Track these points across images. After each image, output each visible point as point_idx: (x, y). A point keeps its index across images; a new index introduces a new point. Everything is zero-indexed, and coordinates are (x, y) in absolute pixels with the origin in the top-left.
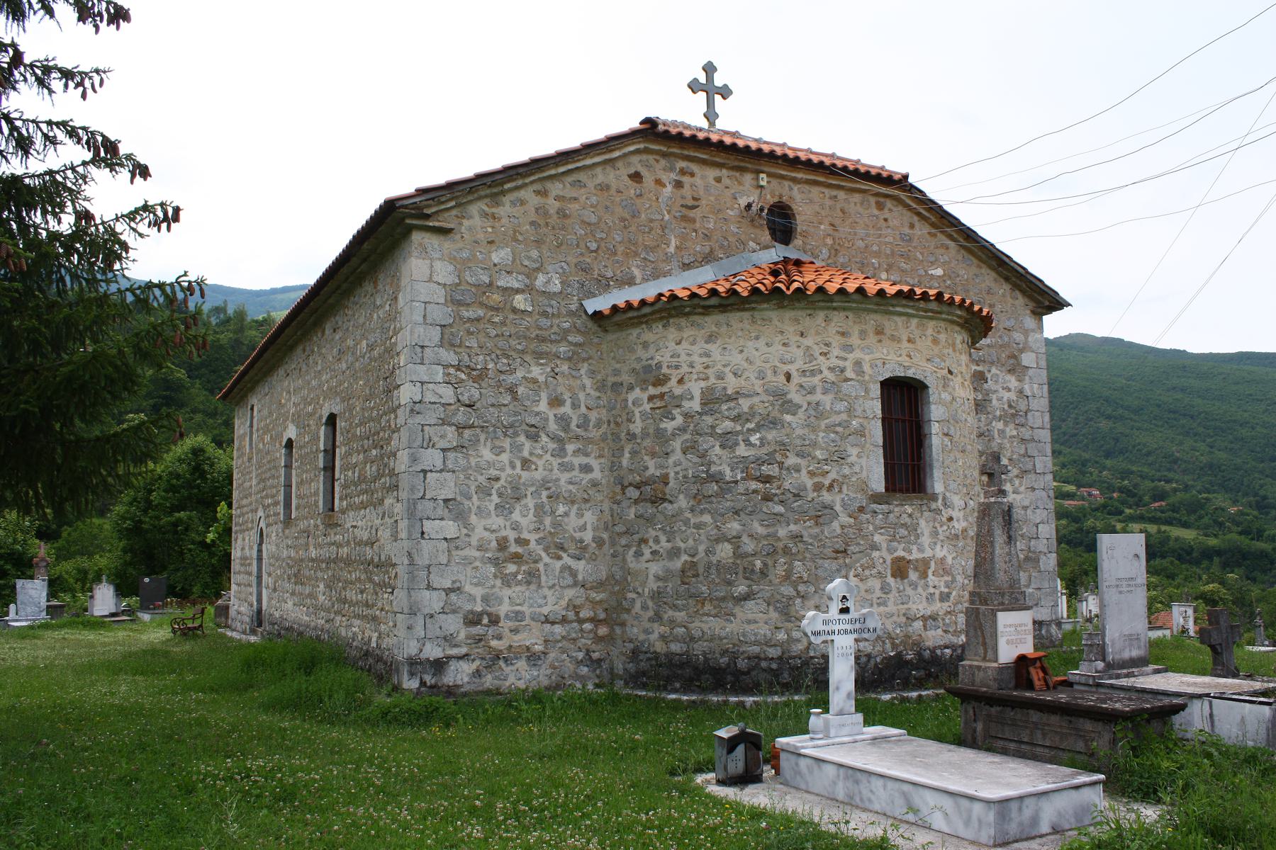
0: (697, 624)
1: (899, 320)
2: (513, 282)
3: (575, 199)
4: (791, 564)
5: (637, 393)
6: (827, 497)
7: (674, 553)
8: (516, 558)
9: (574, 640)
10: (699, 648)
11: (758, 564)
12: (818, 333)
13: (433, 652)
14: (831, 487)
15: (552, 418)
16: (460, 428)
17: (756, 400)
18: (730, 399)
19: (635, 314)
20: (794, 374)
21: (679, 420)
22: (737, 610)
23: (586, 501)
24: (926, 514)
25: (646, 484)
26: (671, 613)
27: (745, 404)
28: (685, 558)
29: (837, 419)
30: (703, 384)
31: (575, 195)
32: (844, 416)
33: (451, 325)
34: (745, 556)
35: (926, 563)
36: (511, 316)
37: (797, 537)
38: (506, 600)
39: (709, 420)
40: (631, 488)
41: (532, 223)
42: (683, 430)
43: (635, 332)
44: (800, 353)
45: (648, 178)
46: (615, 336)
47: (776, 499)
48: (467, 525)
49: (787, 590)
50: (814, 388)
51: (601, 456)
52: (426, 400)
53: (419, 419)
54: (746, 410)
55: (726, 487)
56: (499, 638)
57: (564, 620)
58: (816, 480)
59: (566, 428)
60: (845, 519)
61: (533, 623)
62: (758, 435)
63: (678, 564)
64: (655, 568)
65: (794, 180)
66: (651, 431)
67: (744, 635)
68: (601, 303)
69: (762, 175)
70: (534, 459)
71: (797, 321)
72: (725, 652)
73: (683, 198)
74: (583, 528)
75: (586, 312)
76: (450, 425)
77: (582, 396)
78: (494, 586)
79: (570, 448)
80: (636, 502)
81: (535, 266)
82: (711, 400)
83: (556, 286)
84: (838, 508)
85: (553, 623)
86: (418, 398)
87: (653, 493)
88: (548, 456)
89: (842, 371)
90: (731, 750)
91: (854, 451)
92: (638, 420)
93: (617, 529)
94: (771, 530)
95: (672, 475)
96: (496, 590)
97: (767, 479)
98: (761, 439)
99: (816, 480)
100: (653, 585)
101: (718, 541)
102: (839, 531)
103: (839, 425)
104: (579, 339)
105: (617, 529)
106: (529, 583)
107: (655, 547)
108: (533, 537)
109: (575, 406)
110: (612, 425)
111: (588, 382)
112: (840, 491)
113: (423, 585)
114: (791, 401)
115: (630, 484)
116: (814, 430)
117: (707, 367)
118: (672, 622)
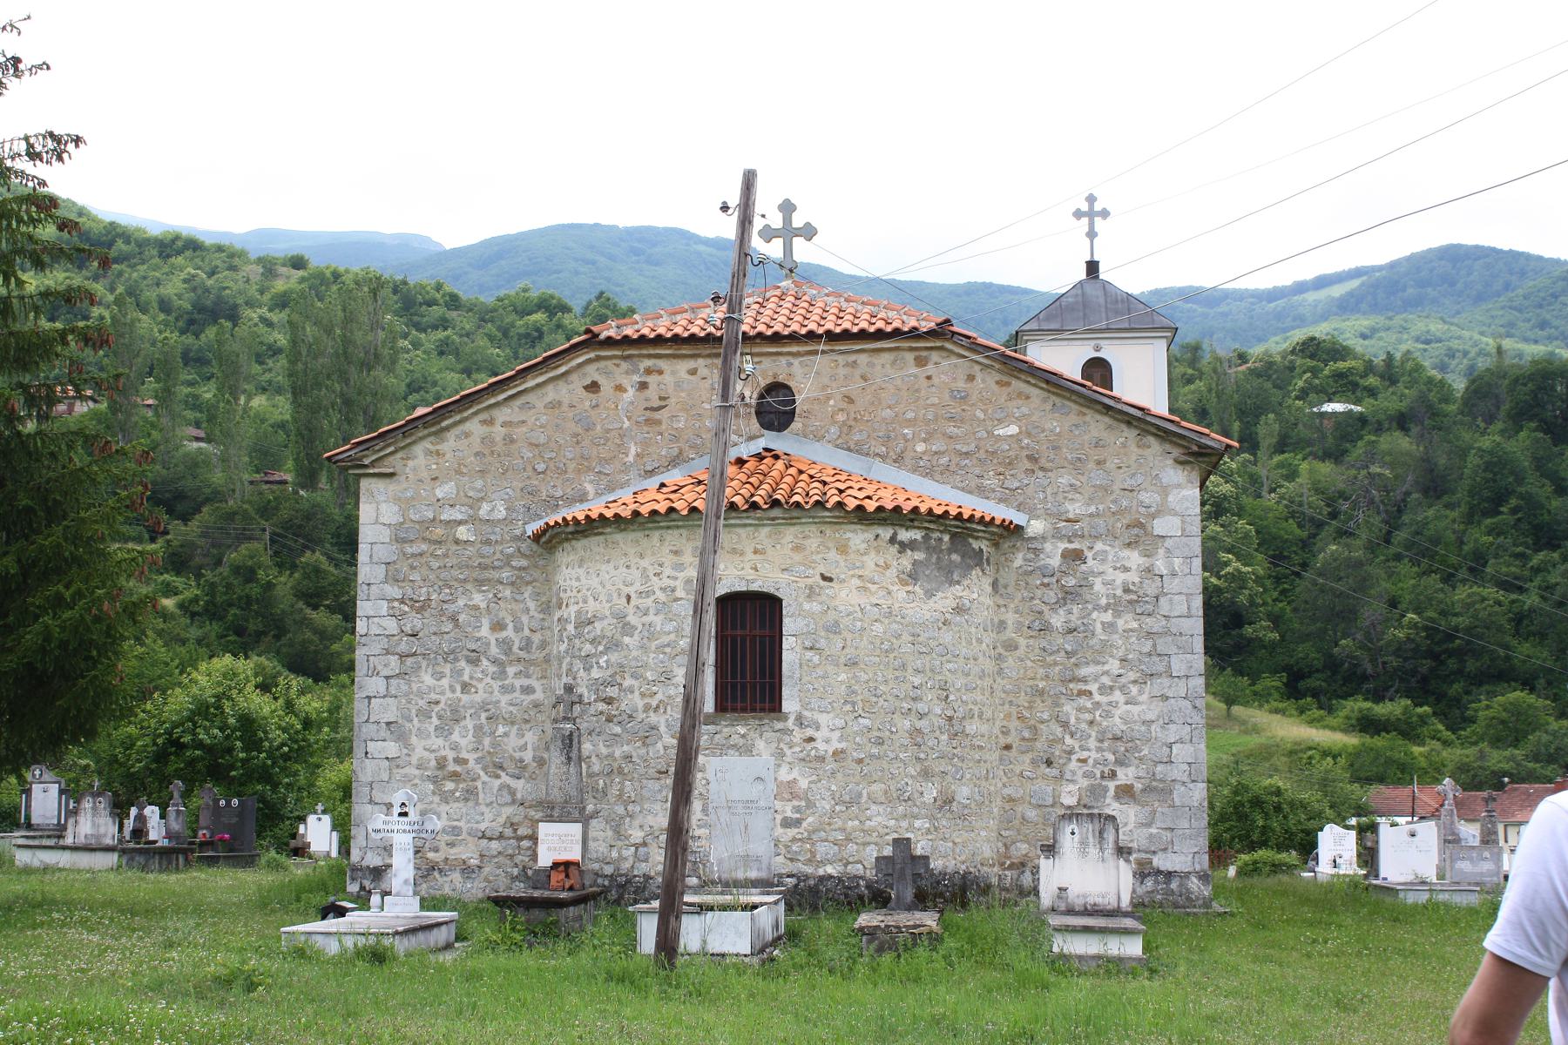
12: (653, 554)
14: (657, 709)
16: (403, 656)
20: (633, 596)
23: (527, 721)
29: (665, 639)
32: (672, 636)
36: (455, 547)
48: (407, 745)
70: (474, 683)
74: (524, 748)
97: (609, 701)
106: (466, 800)
109: (518, 629)
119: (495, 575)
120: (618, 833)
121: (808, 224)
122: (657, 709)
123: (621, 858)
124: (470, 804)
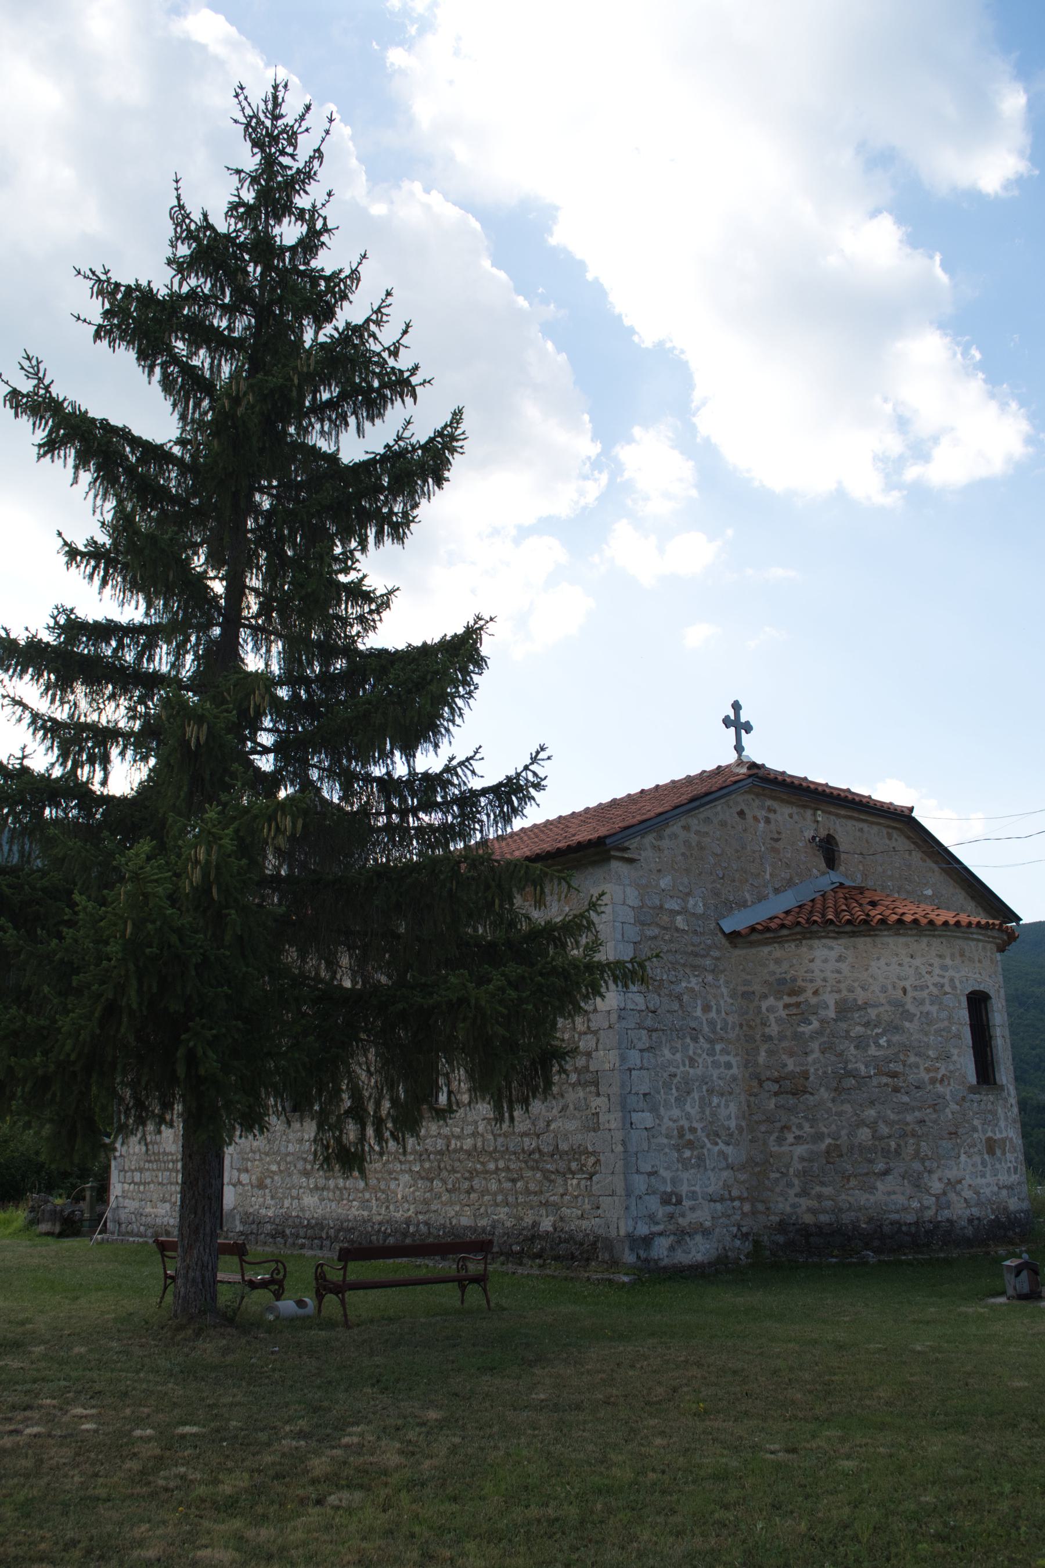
0: (844, 1197)
1: (973, 944)
2: (673, 905)
3: (707, 833)
4: (918, 1145)
5: (771, 1001)
6: (940, 1088)
7: (819, 1137)
8: (690, 1145)
9: (729, 1216)
10: (847, 1218)
11: (893, 1144)
12: (923, 956)
13: (643, 1230)
14: (942, 1081)
15: (705, 1022)
16: (651, 1030)
17: (881, 1009)
18: (860, 1008)
19: (772, 935)
20: (909, 989)
21: (816, 1025)
22: (879, 1184)
23: (730, 1094)
24: (1001, 1102)
25: (785, 1078)
26: (818, 1189)
27: (873, 1013)
28: (828, 1141)
29: (941, 1025)
30: (837, 996)
31: (706, 830)
32: (946, 1023)
33: (639, 943)
34: (881, 1138)
35: (1004, 1140)
36: (676, 935)
37: (921, 1122)
38: (685, 1181)
39: (844, 1026)
40: (769, 1083)
41: (683, 854)
42: (819, 1033)
43: (766, 950)
44: (912, 971)
45: (749, 815)
46: (744, 952)
47: (903, 1090)
48: (659, 1117)
49: (917, 1166)
50: (924, 1000)
51: (737, 1055)
52: (628, 1007)
53: (624, 1024)
54: (874, 1017)
55: (862, 1081)
56: (683, 1215)
57: (722, 1200)
58: (932, 1075)
59: (714, 1032)
60: (954, 1107)
61: (703, 1202)
62: (885, 1038)
63: (823, 1146)
64: (800, 1150)
65: (838, 815)
66: (788, 1034)
67: (886, 1205)
68: (737, 922)
69: (819, 812)
70: (696, 1058)
71: (907, 945)
72: (870, 1220)
73: (771, 832)
74: (729, 1118)
75: (723, 932)
76: (644, 1028)
77: (722, 1002)
78: (678, 1170)
79: (718, 1047)
80: (776, 1094)
81: (687, 890)
82: (844, 1009)
83: (700, 910)
84: (948, 1097)
85: (715, 1201)
86: (622, 1006)
87: (793, 1087)
88: (704, 1055)
89: (942, 986)
90: (1018, 1275)
91: (955, 1051)
92: (773, 1024)
93: (755, 1118)
94: (901, 1116)
95: (812, 1070)
96: (679, 1173)
97: (894, 1075)
98: (888, 1041)
99: (932, 1075)
100: (797, 1165)
101: (858, 1126)
102: (950, 1116)
103: (943, 1030)
104: (717, 954)
105: (755, 1118)
106: (699, 1166)
107: (798, 1133)
108: (698, 1126)
109: (718, 1012)
110: (745, 1028)
111: (724, 990)
112: (949, 1084)
113: (634, 1170)
114: (908, 1011)
115: (768, 1079)
116: (926, 1034)
117: (839, 982)
118: (819, 1197)
119: (699, 961)
120: (918, 1185)
121: (748, 722)
122: (942, 1081)
123: (924, 1208)
124: (702, 1169)
